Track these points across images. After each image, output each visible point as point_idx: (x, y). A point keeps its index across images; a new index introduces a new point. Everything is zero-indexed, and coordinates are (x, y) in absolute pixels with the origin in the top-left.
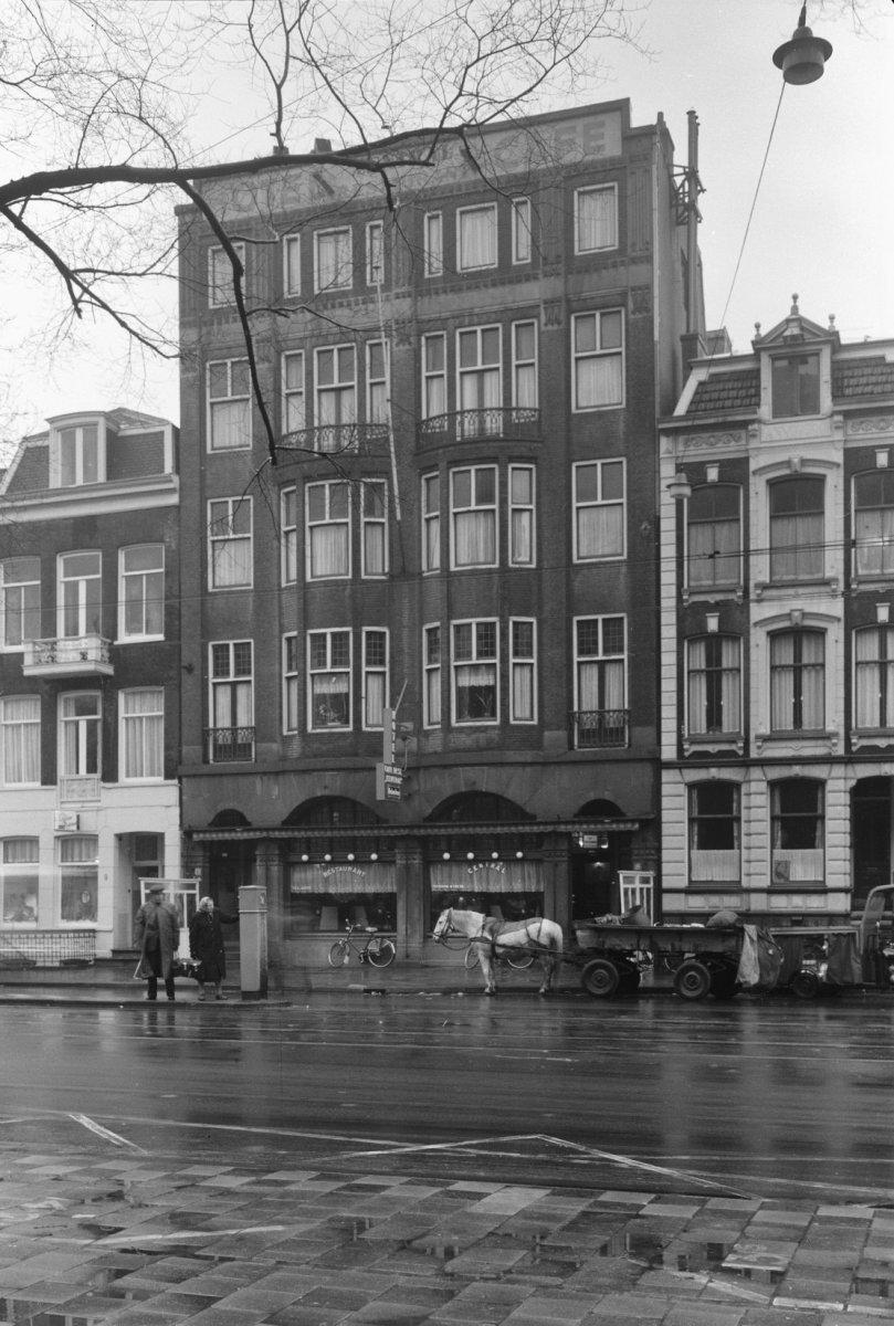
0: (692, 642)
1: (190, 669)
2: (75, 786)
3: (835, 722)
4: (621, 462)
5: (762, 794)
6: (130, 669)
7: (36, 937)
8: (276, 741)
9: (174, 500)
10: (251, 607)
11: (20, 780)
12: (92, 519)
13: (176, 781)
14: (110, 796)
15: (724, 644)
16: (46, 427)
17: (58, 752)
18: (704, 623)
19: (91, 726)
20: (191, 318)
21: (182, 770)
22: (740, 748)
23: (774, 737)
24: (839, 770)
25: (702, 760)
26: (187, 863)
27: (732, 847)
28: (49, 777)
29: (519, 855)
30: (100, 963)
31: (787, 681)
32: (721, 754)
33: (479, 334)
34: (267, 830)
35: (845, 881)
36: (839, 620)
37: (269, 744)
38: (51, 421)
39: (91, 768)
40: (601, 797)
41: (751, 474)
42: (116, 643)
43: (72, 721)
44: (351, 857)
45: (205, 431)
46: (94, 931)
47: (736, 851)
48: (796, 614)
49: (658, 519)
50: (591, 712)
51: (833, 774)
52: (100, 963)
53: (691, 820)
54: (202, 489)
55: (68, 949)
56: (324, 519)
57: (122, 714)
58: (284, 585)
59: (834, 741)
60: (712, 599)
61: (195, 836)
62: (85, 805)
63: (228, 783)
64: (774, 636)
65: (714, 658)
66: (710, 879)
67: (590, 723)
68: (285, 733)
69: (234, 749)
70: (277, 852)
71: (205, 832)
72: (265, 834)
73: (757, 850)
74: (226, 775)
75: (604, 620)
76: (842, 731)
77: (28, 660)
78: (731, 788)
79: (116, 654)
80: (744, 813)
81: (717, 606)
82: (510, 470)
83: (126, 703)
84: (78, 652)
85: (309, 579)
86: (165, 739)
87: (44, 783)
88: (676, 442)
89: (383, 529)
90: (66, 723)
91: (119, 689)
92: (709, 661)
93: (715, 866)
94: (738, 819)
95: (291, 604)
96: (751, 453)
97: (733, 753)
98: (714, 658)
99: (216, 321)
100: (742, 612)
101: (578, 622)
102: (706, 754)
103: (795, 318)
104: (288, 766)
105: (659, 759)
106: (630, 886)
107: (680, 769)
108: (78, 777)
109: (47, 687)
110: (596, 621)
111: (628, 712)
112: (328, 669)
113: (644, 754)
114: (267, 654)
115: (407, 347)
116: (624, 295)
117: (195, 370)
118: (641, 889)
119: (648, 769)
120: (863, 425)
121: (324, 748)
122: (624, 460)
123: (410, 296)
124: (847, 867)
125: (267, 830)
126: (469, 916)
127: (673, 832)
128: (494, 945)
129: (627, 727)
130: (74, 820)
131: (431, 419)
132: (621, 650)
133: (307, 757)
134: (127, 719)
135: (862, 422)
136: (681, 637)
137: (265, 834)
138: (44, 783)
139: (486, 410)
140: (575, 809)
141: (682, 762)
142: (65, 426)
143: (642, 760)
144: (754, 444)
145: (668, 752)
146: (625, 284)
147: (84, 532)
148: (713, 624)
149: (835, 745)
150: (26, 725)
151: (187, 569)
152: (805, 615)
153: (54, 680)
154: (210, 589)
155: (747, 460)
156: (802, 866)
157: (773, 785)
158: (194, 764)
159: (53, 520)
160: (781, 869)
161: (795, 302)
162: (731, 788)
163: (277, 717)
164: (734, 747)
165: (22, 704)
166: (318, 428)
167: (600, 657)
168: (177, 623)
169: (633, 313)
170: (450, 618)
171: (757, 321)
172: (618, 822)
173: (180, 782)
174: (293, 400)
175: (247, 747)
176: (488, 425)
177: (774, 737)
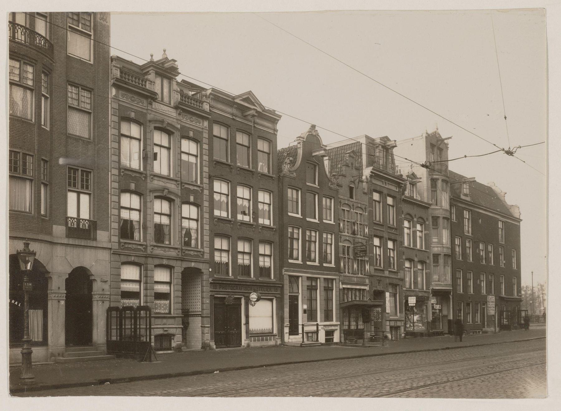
24: (179, 263)
48: (167, 191)
152: (170, 192)
167: (80, 190)
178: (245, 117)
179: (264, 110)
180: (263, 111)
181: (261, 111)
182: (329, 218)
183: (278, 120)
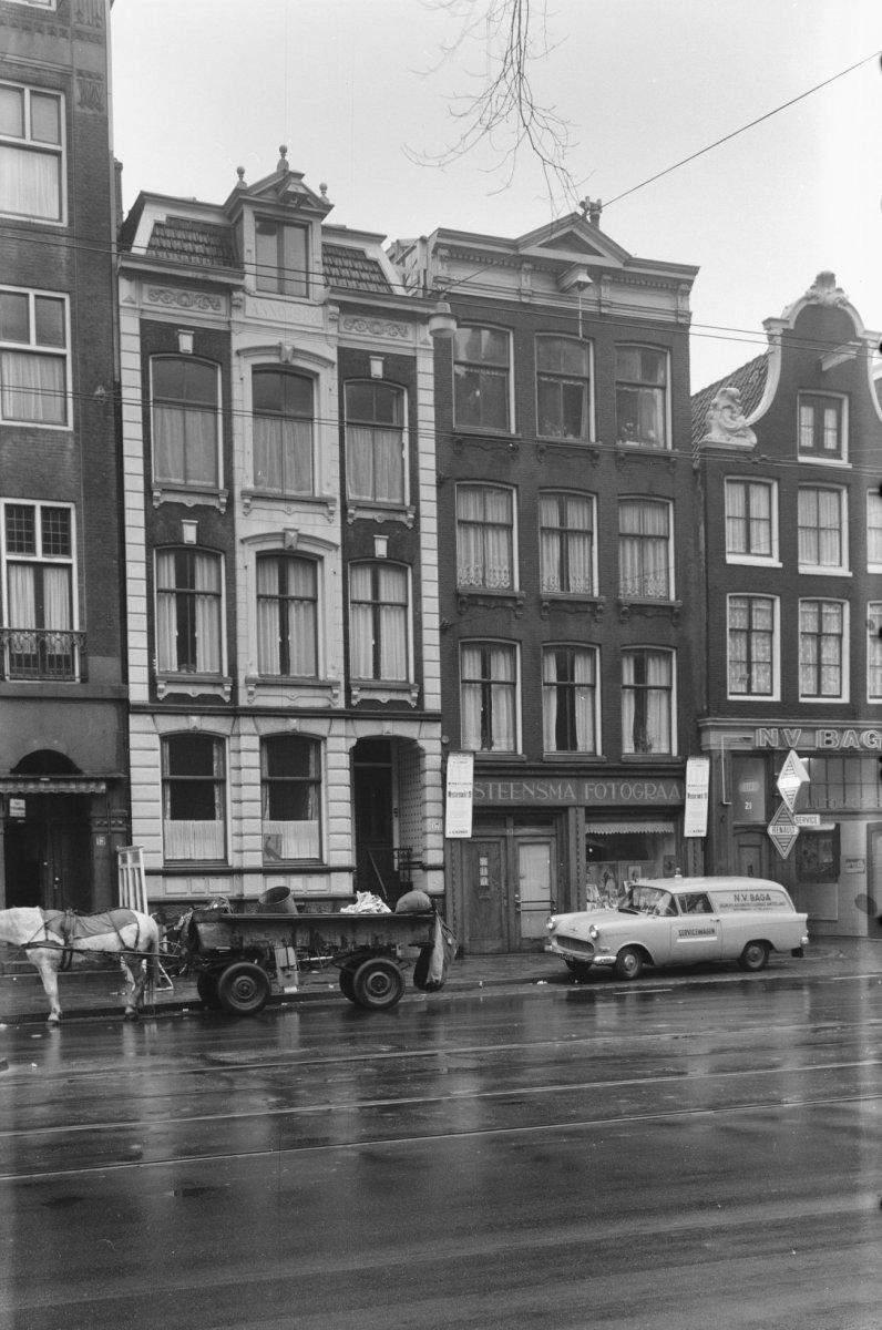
0: (161, 553)
3: (332, 670)
5: (254, 751)
15: (198, 560)
18: (178, 532)
22: (226, 693)
23: (263, 683)
24: (339, 727)
25: (179, 705)
27: (212, 817)
31: (273, 613)
32: (203, 698)
35: (347, 858)
36: (336, 546)
40: (48, 746)
41: (233, 354)
47: (218, 823)
48: (293, 534)
49: (118, 387)
51: (333, 732)
53: (263, 782)
59: (335, 691)
60: (190, 501)
64: (262, 558)
65: (185, 576)
66: (188, 857)
67: (28, 646)
73: (246, 816)
76: (342, 679)
78: (214, 741)
80: (231, 777)
81: (197, 512)
88: (140, 289)
89: (65, 365)
92: (179, 582)
93: (197, 840)
94: (222, 782)
96: (235, 327)
97: (217, 698)
98: (185, 576)
100: (225, 524)
102: (183, 698)
103: (286, 175)
105: (127, 700)
107: (152, 714)
111: (80, 635)
113: (109, 694)
116: (66, 75)
119: (109, 715)
120: (356, 324)
124: (348, 841)
126: (17, 917)
127: (145, 796)
128: (69, 950)
135: (355, 320)
136: (151, 544)
141: (155, 708)
143: (103, 701)
144: (237, 316)
145: (138, 693)
146: (68, 62)
148: (381, 548)
149: (336, 696)
152: (301, 538)
155: (228, 334)
156: (297, 841)
157: (267, 741)
160: (272, 845)
161: (283, 155)
162: (214, 741)
164: (218, 691)
167: (39, 557)
171: (325, 182)
175: (67, 661)
177: (263, 683)
178: (564, 291)
179: (629, 261)
180: (625, 265)
181: (619, 265)
182: (830, 443)
183: (690, 283)
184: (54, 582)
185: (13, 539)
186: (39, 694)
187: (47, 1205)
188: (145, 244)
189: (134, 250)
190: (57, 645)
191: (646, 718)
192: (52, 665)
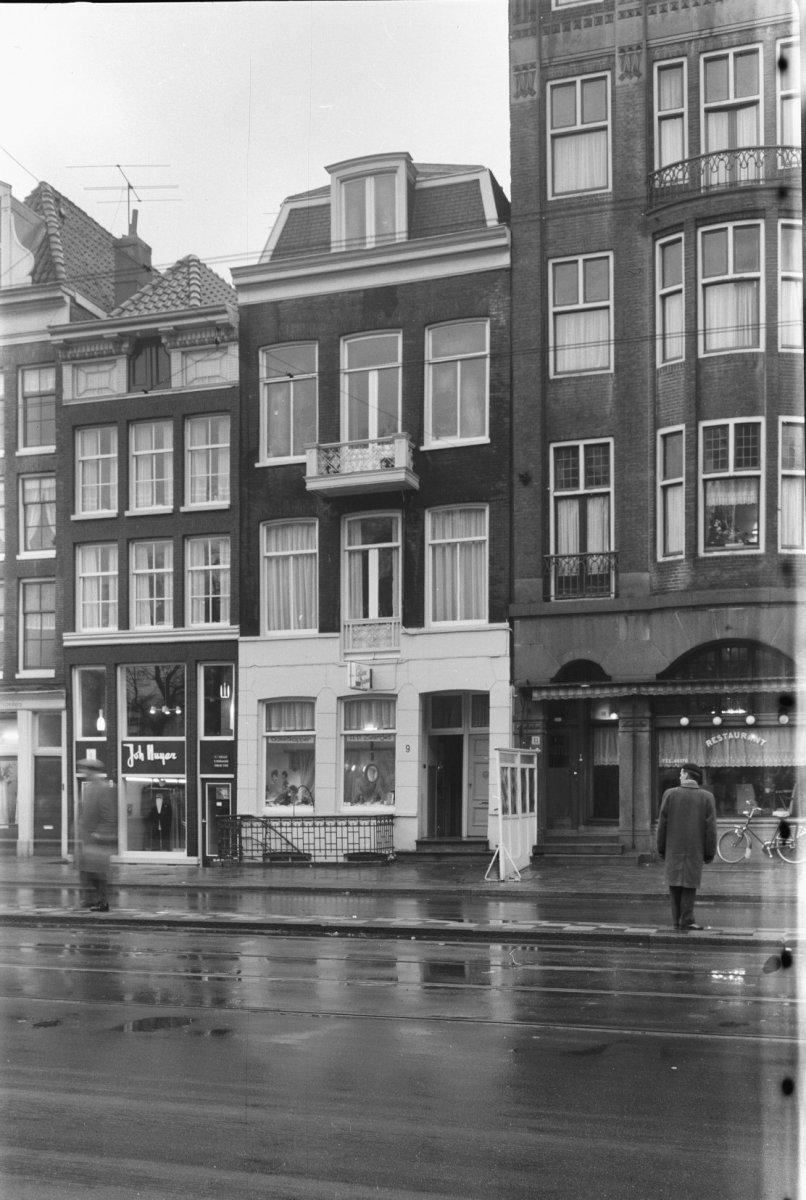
1: (526, 480)
2: (364, 633)
4: (607, 258)
6: (441, 481)
7: (325, 826)
8: (647, 571)
9: (504, 260)
10: (610, 398)
11: (287, 627)
12: (390, 291)
13: (506, 625)
14: (412, 645)
16: (326, 180)
17: (342, 593)
19: (386, 556)
20: (528, 25)
21: (514, 610)
26: (521, 729)
28: (329, 621)
29: (684, 721)
30: (403, 858)
33: (731, 57)
34: (638, 685)
37: (635, 575)
38: (330, 169)
39: (386, 609)
42: (422, 449)
43: (358, 551)
44: (684, 721)
45: (545, 177)
46: (392, 817)
50: (570, 556)
52: (403, 857)
54: (543, 246)
55: (366, 840)
56: (727, 273)
57: (429, 540)
58: (659, 365)
61: (536, 695)
62: (377, 657)
63: (579, 625)
67: (570, 568)
68: (660, 559)
69: (584, 581)
70: (541, 718)
71: (548, 689)
72: (634, 691)
74: (578, 615)
75: (737, 426)
77: (312, 470)
79: (422, 460)
82: (779, 227)
83: (434, 523)
84: (372, 460)
85: (701, 355)
86: (490, 569)
87: (322, 630)
90: (351, 553)
91: (426, 507)
95: (675, 392)
99: (561, 28)
101: (555, 449)
104: (670, 601)
106: (528, 766)
108: (365, 621)
109: (327, 508)
110: (726, 427)
111: (615, 555)
112: (731, 472)
114: (635, 455)
115: (635, 79)
117: (532, 93)
118: (523, 771)
121: (726, 576)
122: (610, 254)
123: (639, 14)
125: (638, 685)
129: (613, 573)
130: (367, 676)
131: (665, 169)
132: (606, 482)
133: (701, 588)
134: (434, 547)
137: (634, 691)
138: (322, 630)
139: (740, 150)
140: (554, 671)
142: (350, 174)
147: (379, 309)
150: (296, 557)
151: (520, 355)
153: (337, 499)
154: (552, 376)
158: (531, 602)
159: (336, 294)
163: (650, 538)
165: (289, 532)
166: (659, 172)
167: (582, 491)
168: (507, 420)
169: (622, 78)
170: (700, 417)
172: (602, 687)
173: (512, 626)
174: (668, 125)
175: (604, 579)
176: (609, 200)
184: (594, 509)
185: (722, 461)
186: (573, 611)
187: (229, 1031)
188: (373, 233)
189: (489, 224)
190: (595, 566)
191: (692, 650)
192: (567, 585)
